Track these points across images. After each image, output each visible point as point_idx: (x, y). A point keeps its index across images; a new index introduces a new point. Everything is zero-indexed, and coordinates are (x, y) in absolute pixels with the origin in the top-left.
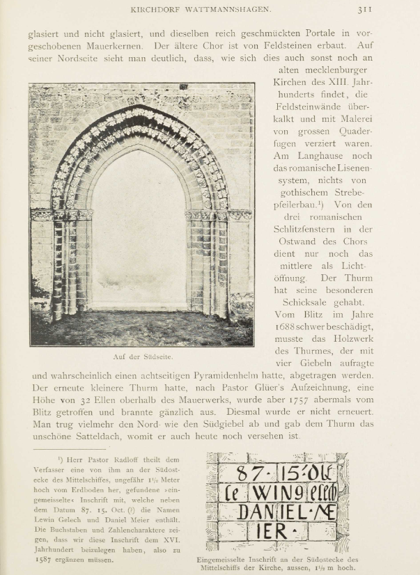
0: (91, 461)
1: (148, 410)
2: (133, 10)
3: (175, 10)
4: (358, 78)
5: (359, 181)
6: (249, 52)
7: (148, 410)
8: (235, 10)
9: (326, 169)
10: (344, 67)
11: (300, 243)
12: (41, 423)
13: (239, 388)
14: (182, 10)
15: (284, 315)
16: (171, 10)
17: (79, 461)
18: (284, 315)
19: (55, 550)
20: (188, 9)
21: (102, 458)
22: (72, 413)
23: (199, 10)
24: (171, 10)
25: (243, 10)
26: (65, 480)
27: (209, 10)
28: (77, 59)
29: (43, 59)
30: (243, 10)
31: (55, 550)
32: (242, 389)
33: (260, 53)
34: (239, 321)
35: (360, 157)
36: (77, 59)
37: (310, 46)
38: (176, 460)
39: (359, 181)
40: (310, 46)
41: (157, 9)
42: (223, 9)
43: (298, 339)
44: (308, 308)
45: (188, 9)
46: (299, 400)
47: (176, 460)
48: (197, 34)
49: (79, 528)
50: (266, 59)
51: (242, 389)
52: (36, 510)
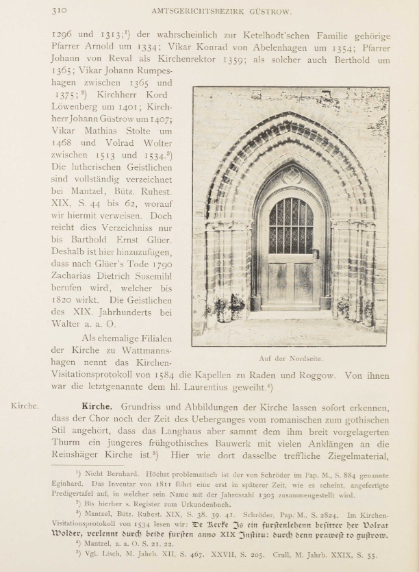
0: (55, 494)
1: (139, 385)
4: (106, 161)
7: (139, 385)
9: (106, 168)
11: (57, 388)
12: (92, 129)
15: (355, 376)
16: (161, 11)
17: (133, 95)
18: (355, 376)
19: (196, 505)
21: (112, 372)
24: (161, 11)
26: (136, 70)
31: (196, 505)
34: (303, 132)
35: (121, 419)
43: (368, 457)
44: (89, 125)
46: (70, 94)
48: (269, 457)
49: (217, 503)
52: (55, 264)
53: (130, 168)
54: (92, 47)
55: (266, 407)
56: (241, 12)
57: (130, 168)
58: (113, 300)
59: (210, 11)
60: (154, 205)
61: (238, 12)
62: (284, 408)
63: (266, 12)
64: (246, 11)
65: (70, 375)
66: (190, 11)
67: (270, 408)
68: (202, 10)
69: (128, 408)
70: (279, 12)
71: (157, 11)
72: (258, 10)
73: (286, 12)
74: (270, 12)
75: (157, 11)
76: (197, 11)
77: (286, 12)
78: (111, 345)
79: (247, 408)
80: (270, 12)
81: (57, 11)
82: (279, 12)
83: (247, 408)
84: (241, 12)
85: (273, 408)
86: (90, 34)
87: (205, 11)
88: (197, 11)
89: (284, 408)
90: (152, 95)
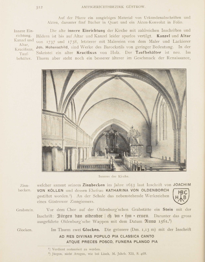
2: (107, 190)
22: (58, 202)
53: (136, 58)
54: (80, 196)
55: (118, 30)
56: (122, 7)
57: (136, 58)
58: (106, 230)
59: (108, 7)
60: (131, 42)
61: (121, 7)
62: (126, 31)
63: (134, 7)
64: (125, 7)
65: (24, 45)
66: (99, 7)
67: (120, 31)
68: (104, 6)
69: (135, 210)
70: (140, 7)
71: (84, 7)
72: (130, 6)
73: (143, 7)
74: (136, 7)
75: (84, 7)
76: (102, 7)
77: (143, 7)
78: (88, 199)
79: (109, 31)
80: (136, 7)
81: (38, 7)
82: (140, 7)
83: (109, 31)
84: (122, 7)
85: (121, 31)
86: (140, 18)
87: (106, 7)
88: (102, 7)
89: (126, 31)
90: (151, 22)
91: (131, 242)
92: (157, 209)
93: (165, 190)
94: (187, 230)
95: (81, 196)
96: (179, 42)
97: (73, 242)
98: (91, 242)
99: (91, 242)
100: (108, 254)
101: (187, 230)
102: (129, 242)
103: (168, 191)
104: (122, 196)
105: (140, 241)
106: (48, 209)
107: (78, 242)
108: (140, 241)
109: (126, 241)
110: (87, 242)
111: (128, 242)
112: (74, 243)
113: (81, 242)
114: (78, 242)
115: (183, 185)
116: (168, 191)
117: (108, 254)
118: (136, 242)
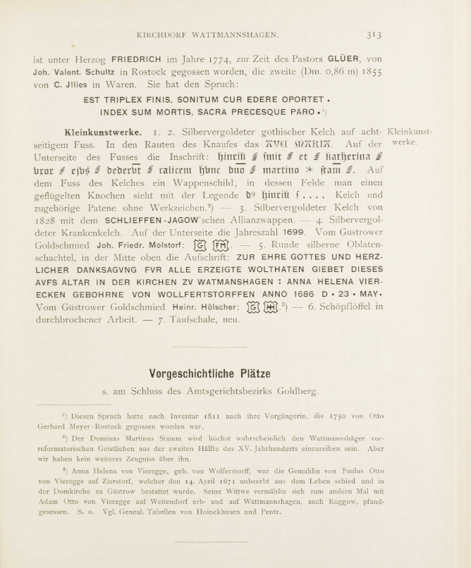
0: (296, 60)
2: (138, 35)
3: (181, 35)
5: (223, 72)
6: (316, 497)
8: (242, 35)
10: (68, 243)
13: (309, 60)
14: (189, 35)
20: (195, 35)
23: (206, 35)
25: (250, 36)
27: (216, 35)
28: (284, 449)
29: (92, 320)
30: (250, 36)
32: (312, 60)
33: (272, 476)
36: (284, 449)
37: (328, 482)
38: (379, 59)
39: (223, 72)
40: (328, 482)
41: (164, 34)
42: (229, 35)
45: (195, 35)
47: (379, 59)
50: (220, 233)
51: (312, 60)
91: (224, 112)
92: (160, 181)
93: (155, 282)
94: (195, 158)
95: (157, 85)
96: (159, 73)
97: (270, 112)
98: (252, 112)
99: (252, 112)
100: (239, 417)
101: (195, 158)
102: (221, 112)
103: (158, 61)
104: (122, 320)
105: (265, 292)
106: (40, 306)
107: (282, 112)
108: (265, 292)
109: (265, 99)
110: (243, 112)
111: (218, 113)
112: (273, 114)
113: (288, 112)
114: (282, 112)
115: (155, 59)
116: (158, 61)
117: (239, 417)
118: (125, 100)
